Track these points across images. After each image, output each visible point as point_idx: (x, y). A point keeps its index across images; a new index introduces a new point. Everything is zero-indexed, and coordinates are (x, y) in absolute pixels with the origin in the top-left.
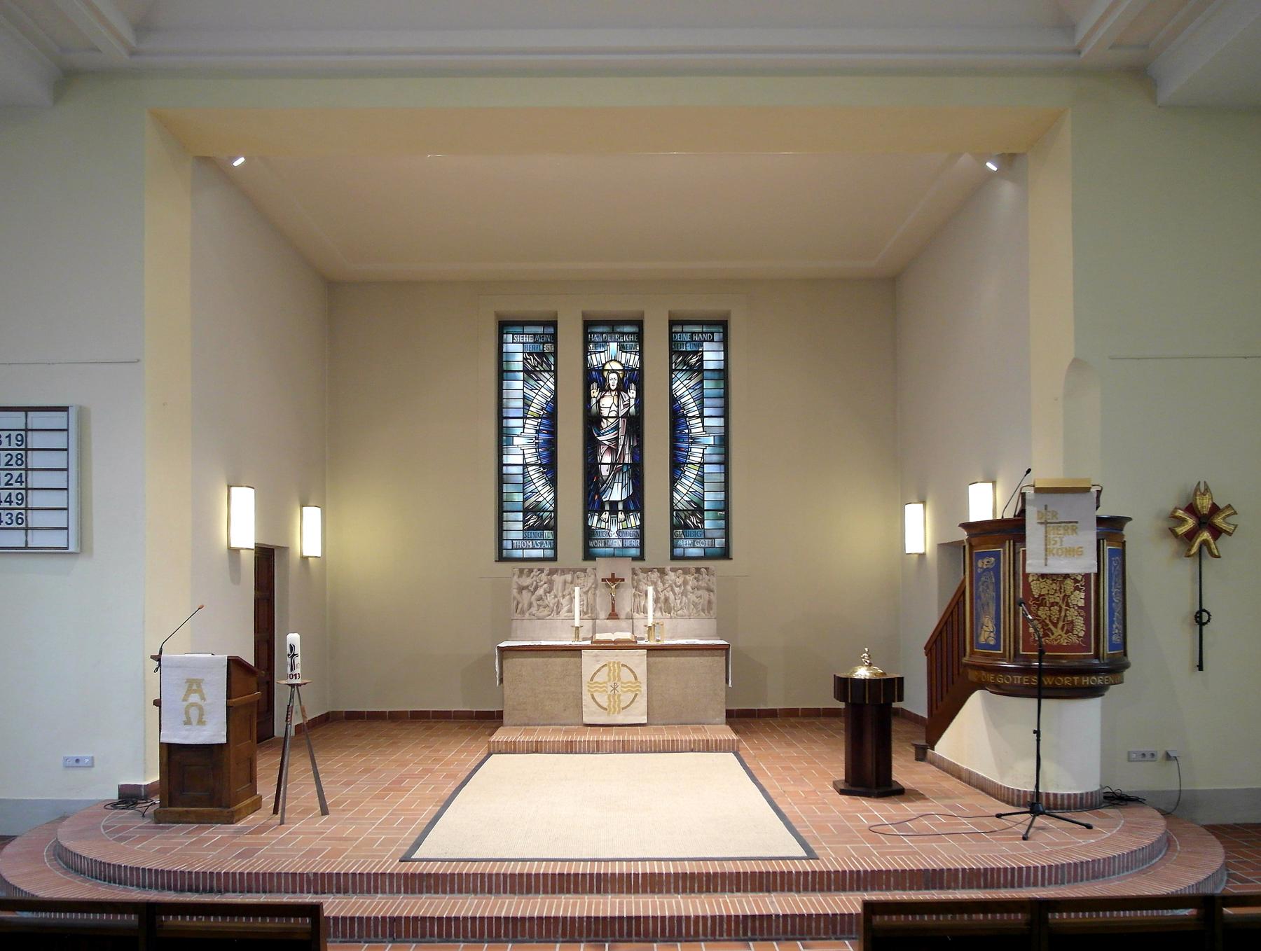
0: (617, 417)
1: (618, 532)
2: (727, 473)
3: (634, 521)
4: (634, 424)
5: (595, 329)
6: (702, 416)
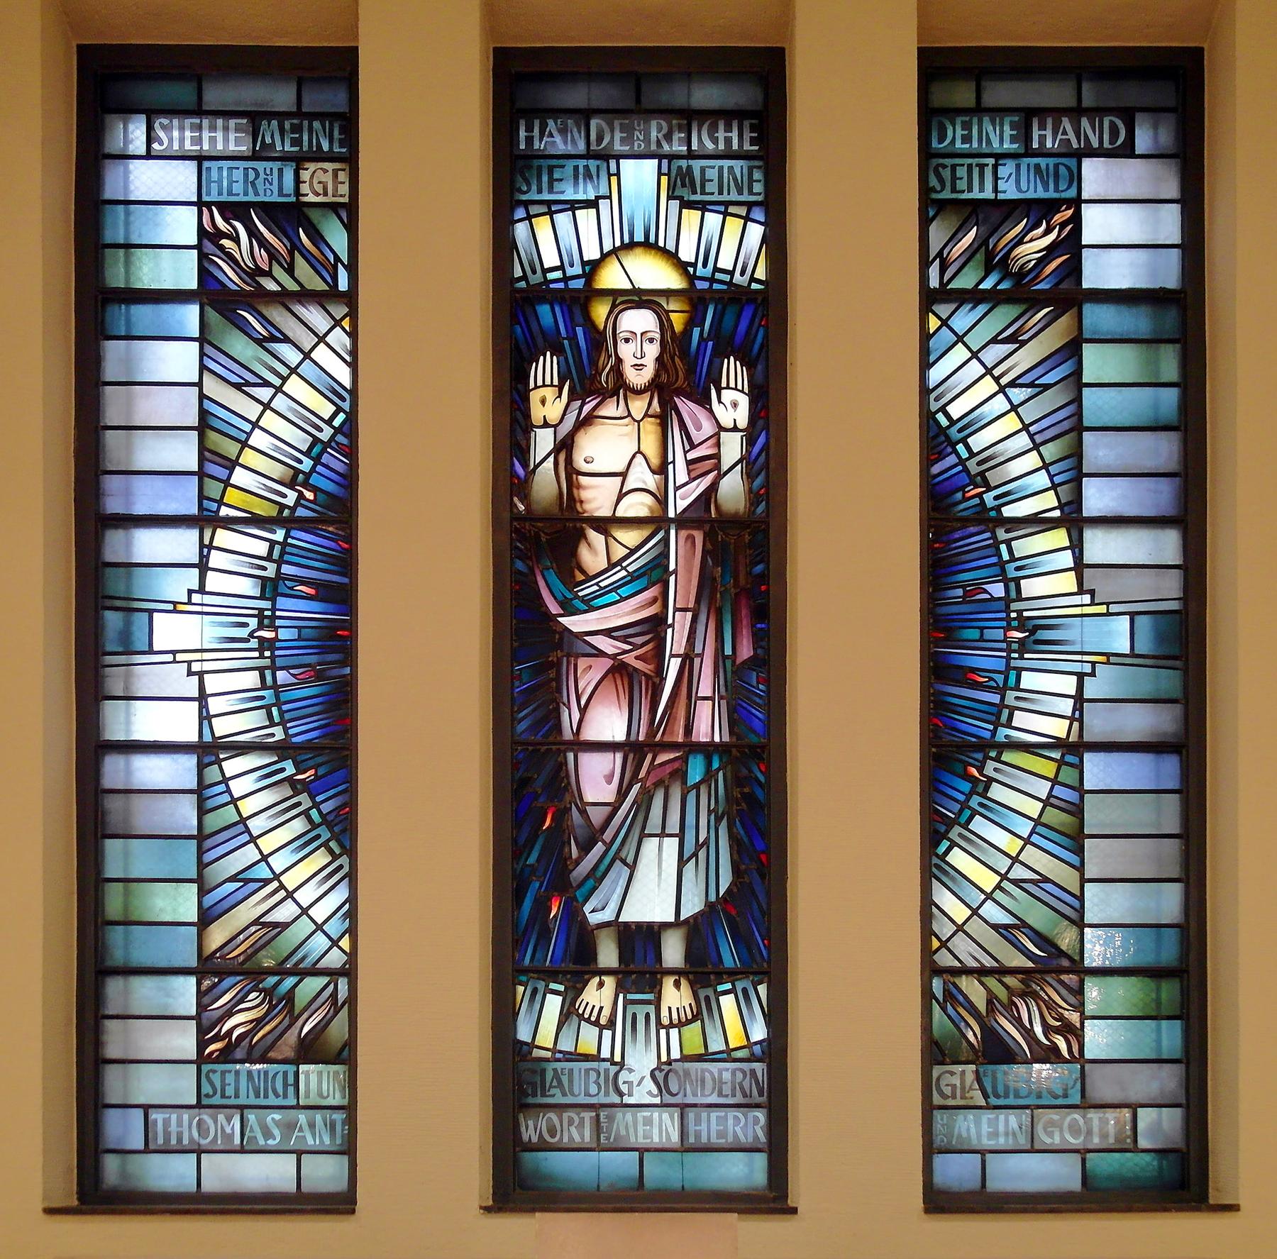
0: (657, 522)
1: (663, 1074)
2: (1192, 794)
3: (738, 1021)
4: (743, 558)
5: (545, 100)
6: (1073, 519)
